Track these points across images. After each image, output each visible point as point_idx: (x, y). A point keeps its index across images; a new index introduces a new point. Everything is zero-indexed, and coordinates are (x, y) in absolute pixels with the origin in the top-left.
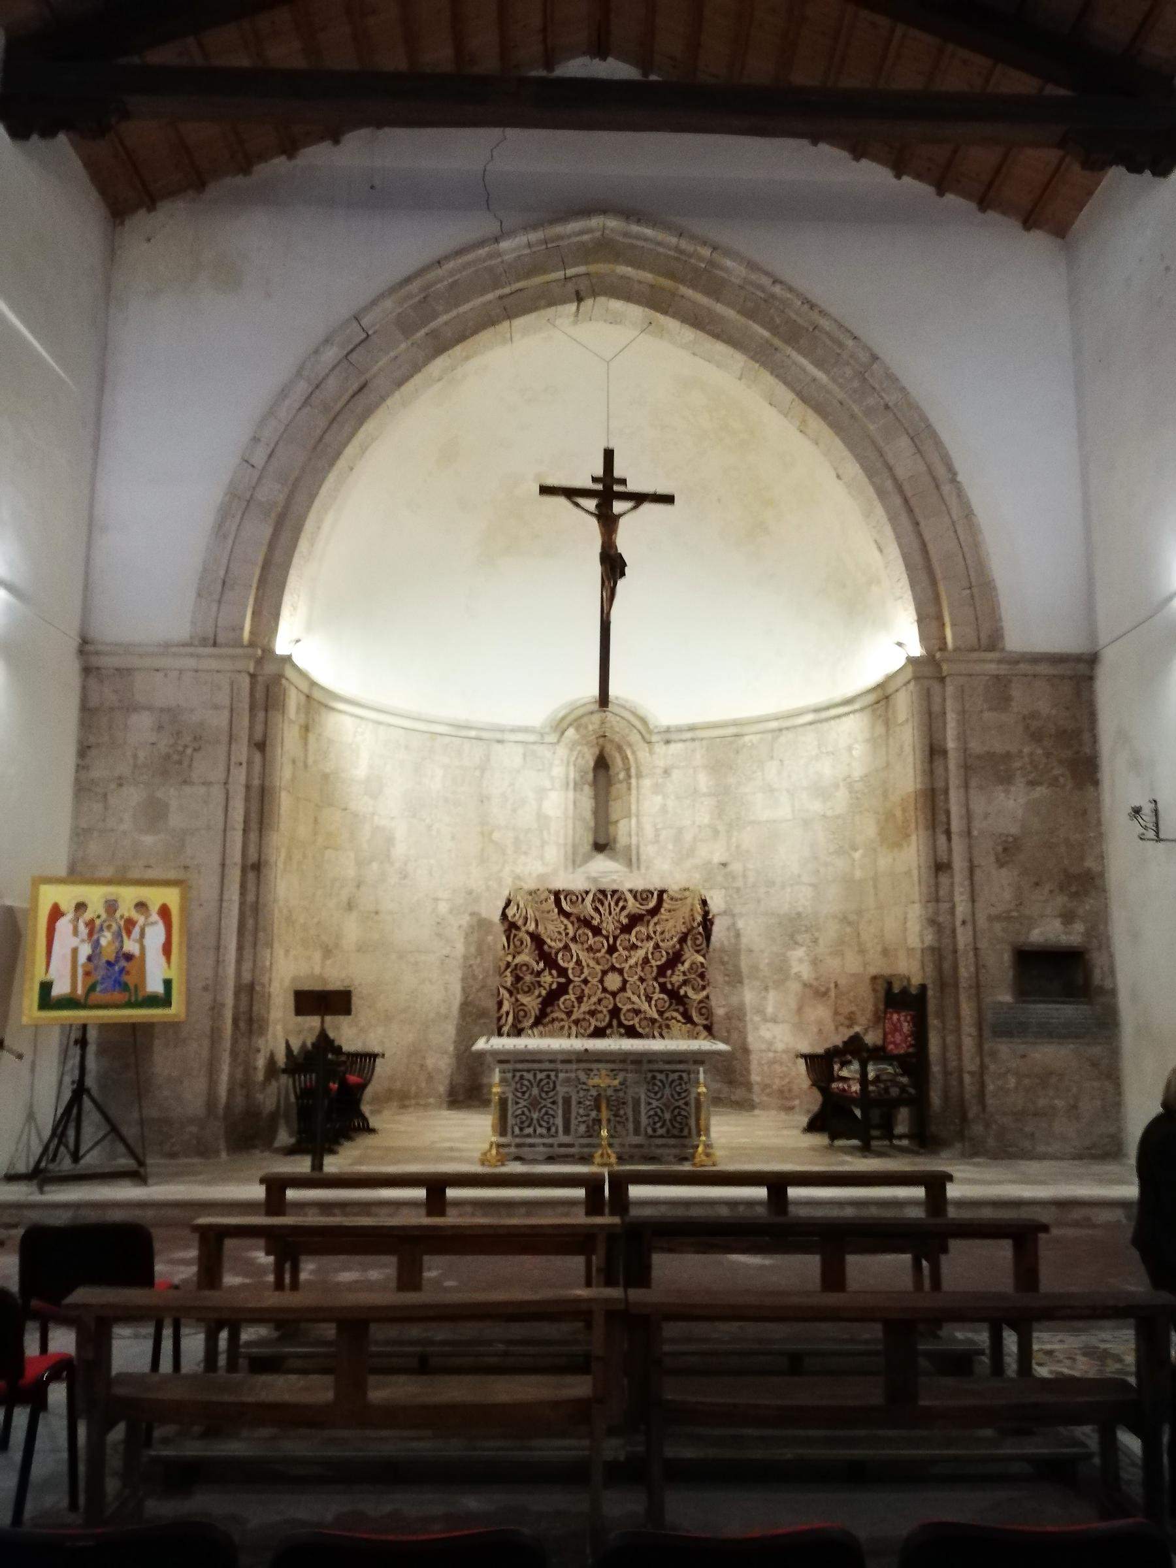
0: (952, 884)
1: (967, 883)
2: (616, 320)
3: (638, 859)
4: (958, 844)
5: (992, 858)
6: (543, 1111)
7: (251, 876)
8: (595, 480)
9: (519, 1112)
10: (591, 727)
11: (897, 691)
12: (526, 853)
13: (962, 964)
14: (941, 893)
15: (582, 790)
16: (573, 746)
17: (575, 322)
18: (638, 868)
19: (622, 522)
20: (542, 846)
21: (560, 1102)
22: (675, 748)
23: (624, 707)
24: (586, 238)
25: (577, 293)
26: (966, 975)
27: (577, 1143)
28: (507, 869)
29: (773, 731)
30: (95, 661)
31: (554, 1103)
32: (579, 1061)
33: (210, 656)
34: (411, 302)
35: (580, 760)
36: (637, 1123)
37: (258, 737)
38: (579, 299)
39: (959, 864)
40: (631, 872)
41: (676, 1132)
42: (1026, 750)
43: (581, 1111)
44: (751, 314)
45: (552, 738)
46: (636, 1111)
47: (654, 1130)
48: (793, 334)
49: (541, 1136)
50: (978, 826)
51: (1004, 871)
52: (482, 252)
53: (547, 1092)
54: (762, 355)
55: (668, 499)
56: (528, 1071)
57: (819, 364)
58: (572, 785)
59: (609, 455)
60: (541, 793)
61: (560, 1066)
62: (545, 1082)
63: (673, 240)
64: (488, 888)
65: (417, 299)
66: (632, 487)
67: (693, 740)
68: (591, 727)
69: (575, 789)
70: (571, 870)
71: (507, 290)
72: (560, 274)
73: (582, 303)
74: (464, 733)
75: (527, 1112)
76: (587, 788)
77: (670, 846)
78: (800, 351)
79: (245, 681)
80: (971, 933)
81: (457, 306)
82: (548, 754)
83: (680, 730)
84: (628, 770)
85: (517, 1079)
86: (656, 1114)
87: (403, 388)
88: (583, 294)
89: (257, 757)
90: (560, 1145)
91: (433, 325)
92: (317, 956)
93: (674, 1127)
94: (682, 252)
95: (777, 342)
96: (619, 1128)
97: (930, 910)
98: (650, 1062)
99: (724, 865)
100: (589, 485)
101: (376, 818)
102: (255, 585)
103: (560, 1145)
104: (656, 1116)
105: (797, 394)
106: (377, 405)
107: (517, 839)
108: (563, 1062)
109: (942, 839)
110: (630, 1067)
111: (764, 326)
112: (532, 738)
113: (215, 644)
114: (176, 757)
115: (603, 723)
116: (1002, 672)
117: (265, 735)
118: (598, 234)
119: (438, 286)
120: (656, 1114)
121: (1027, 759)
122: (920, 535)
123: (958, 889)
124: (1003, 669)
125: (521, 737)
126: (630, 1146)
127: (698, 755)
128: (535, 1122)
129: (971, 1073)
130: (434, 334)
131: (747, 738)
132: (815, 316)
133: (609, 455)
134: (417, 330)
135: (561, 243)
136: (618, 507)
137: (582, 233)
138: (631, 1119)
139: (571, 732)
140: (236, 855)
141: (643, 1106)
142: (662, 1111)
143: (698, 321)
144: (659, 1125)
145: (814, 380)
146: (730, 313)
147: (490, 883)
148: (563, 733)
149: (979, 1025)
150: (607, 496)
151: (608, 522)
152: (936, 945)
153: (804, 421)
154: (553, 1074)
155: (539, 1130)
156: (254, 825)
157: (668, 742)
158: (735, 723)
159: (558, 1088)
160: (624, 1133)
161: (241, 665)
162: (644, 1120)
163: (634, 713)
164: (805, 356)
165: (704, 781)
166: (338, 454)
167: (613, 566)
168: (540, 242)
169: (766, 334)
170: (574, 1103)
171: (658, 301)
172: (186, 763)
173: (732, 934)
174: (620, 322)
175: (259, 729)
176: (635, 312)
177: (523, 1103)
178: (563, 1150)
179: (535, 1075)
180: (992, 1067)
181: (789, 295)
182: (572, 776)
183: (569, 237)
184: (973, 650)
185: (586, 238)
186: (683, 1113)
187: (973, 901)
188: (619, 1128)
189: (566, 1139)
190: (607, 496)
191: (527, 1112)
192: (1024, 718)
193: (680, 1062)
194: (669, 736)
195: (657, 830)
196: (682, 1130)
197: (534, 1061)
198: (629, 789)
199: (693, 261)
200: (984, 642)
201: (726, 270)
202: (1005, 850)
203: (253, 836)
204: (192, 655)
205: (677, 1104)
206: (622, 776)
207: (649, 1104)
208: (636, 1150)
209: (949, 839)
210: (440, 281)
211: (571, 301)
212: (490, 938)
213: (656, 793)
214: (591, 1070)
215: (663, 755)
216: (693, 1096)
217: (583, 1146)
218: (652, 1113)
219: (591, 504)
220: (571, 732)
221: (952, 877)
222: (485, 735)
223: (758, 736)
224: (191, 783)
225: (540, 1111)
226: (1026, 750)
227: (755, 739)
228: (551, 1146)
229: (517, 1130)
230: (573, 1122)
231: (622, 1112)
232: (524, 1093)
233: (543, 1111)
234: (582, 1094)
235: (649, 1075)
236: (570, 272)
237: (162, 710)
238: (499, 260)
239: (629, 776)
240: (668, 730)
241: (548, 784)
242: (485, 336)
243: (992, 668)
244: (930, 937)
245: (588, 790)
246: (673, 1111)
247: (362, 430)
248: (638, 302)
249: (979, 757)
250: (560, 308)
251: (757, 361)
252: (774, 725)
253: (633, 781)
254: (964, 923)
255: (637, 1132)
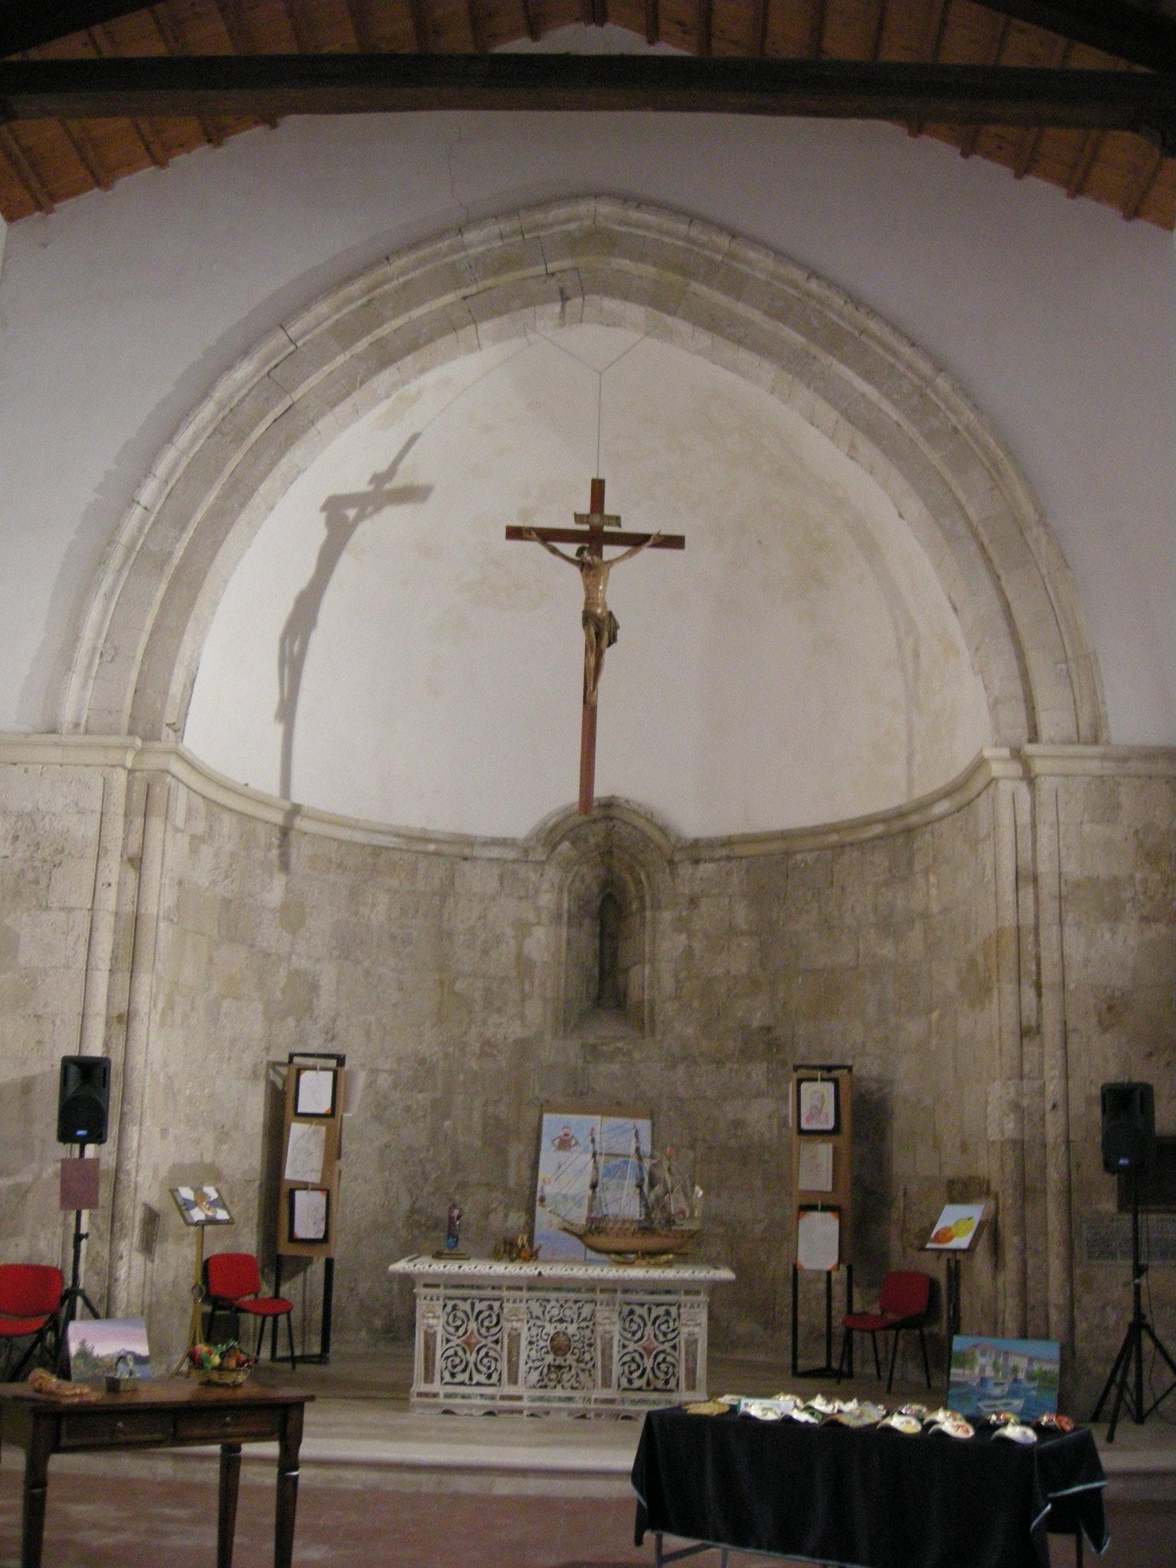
0: (1042, 1055)
1: (1059, 1053)
2: (613, 321)
3: (652, 1020)
4: (1051, 1002)
5: (1093, 1020)
6: (483, 1353)
7: (118, 1030)
8: (579, 518)
9: (451, 1352)
10: (592, 841)
11: (979, 795)
12: (499, 1010)
13: (1051, 1162)
14: (1027, 1068)
15: (581, 925)
16: (567, 865)
17: (562, 325)
18: (653, 1032)
19: (614, 572)
20: (523, 1001)
21: (506, 1341)
22: (707, 869)
23: (635, 812)
24: (573, 226)
25: (562, 291)
26: (1056, 1176)
27: (526, 1395)
28: (474, 1031)
29: (833, 847)
30: (847, 849)
31: (496, 1342)
32: (530, 1289)
33: (77, 746)
34: (353, 306)
35: (578, 884)
36: (607, 1371)
37: (134, 849)
38: (565, 299)
39: (1051, 1028)
40: (643, 1037)
41: (660, 1384)
42: (1138, 876)
43: (533, 1354)
44: (781, 316)
45: (539, 854)
46: (606, 1355)
47: (630, 1381)
48: (834, 340)
49: (478, 1384)
50: (1074, 977)
51: (1107, 1036)
52: (443, 245)
53: (488, 1328)
54: (795, 364)
55: (675, 542)
56: (465, 1299)
57: (868, 376)
58: (565, 919)
59: (598, 488)
60: (523, 929)
61: (505, 1293)
62: (486, 1314)
63: (683, 228)
64: (446, 1056)
65: (360, 302)
66: (628, 527)
67: (729, 858)
68: (592, 841)
69: (570, 925)
70: (561, 1034)
71: (473, 289)
72: (540, 269)
73: (568, 303)
74: (420, 847)
75: (461, 1353)
76: (587, 921)
77: (696, 1004)
78: (844, 361)
79: (120, 778)
80: (1063, 1120)
81: (408, 308)
82: (533, 877)
83: (711, 844)
84: (642, 898)
85: (449, 1309)
86: (633, 1360)
87: (337, 409)
88: (568, 292)
89: (132, 875)
90: (503, 1398)
91: (378, 333)
92: (209, 1139)
93: (657, 1377)
94: (693, 242)
95: (814, 349)
96: (583, 1377)
97: (1012, 1090)
98: (626, 1291)
99: (769, 1029)
100: (570, 524)
101: (294, 957)
102: (139, 656)
103: (503, 1398)
104: (633, 1364)
105: (842, 413)
106: (304, 431)
107: (488, 990)
108: (509, 1288)
109: (1029, 993)
110: (600, 1297)
111: (795, 326)
112: (511, 854)
113: (87, 732)
114: (30, 875)
115: (608, 835)
116: (1107, 772)
117: (143, 847)
118: (588, 223)
119: (387, 287)
120: (633, 1360)
121: (1139, 888)
122: (1001, 592)
123: (1049, 1062)
124: (1109, 768)
125: (496, 852)
126: (596, 1400)
127: (735, 880)
128: (471, 1365)
129: (1057, 1306)
130: (380, 343)
131: (799, 857)
132: (861, 316)
133: (598, 488)
134: (358, 339)
135: (542, 234)
136: (610, 552)
137: (569, 221)
138: (599, 1365)
139: (565, 846)
140: (99, 1003)
141: (615, 1349)
142: (642, 1357)
143: (714, 323)
144: (636, 1375)
145: (863, 395)
146: (755, 315)
147: (451, 1049)
148: (554, 847)
149: (1070, 1244)
150: (593, 539)
151: (591, 569)
152: (1015, 1135)
153: (853, 446)
154: (496, 1305)
155: (477, 1377)
156: (126, 965)
157: (696, 862)
158: (784, 836)
159: (503, 1322)
160: (590, 1384)
161: (114, 757)
162: (616, 1369)
163: (649, 821)
164: (850, 366)
165: (742, 915)
166: (253, 491)
167: (600, 630)
168: (513, 233)
169: (800, 340)
170: (524, 1343)
171: (661, 300)
172: (43, 883)
173: (775, 1122)
174: (619, 325)
175: (135, 838)
176: (636, 312)
177: (455, 1341)
178: (507, 1404)
179: (473, 1305)
180: (1086, 1299)
181: (827, 293)
182: (566, 906)
183: (551, 225)
184: (1071, 743)
185: (573, 226)
186: (669, 1359)
187: (1067, 1077)
188: (583, 1377)
189: (509, 1389)
190: (593, 539)
191: (461, 1353)
192: (1136, 832)
193: (668, 1292)
194: (697, 850)
195: (678, 982)
196: (667, 1382)
197: (472, 1287)
198: (643, 924)
199: (706, 253)
200: (1085, 732)
201: (749, 263)
202: (1110, 1008)
203: (123, 979)
204: (57, 745)
205: (662, 1347)
206: (635, 906)
207: (624, 1346)
208: (604, 1406)
209: (1039, 995)
210: (389, 280)
211: (551, 300)
212: (447, 1123)
213: (678, 930)
214: (548, 1301)
215: (692, 877)
216: (683, 1337)
217: (533, 1399)
218: (627, 1358)
219: (570, 549)
220: (565, 846)
221: (1042, 1045)
222: (445, 848)
223: (816, 854)
224: (47, 908)
225: (478, 1352)
226: (1138, 876)
227: (810, 858)
228: (493, 1398)
229: (447, 1378)
230: (523, 1368)
231: (587, 1357)
232: (457, 1328)
233: (483, 1353)
234: (534, 1331)
235: (626, 1309)
236: (552, 267)
237: (20, 816)
238: (463, 254)
239: (643, 908)
240: (696, 843)
241: (531, 917)
242: (443, 343)
243: (1094, 766)
244: (1011, 1125)
245: (589, 926)
246: (655, 1358)
247: (284, 460)
248: (640, 302)
249: (1078, 885)
250: (539, 309)
251: (790, 372)
252: (834, 838)
253: (648, 914)
254: (1054, 1106)
255: (606, 1384)
